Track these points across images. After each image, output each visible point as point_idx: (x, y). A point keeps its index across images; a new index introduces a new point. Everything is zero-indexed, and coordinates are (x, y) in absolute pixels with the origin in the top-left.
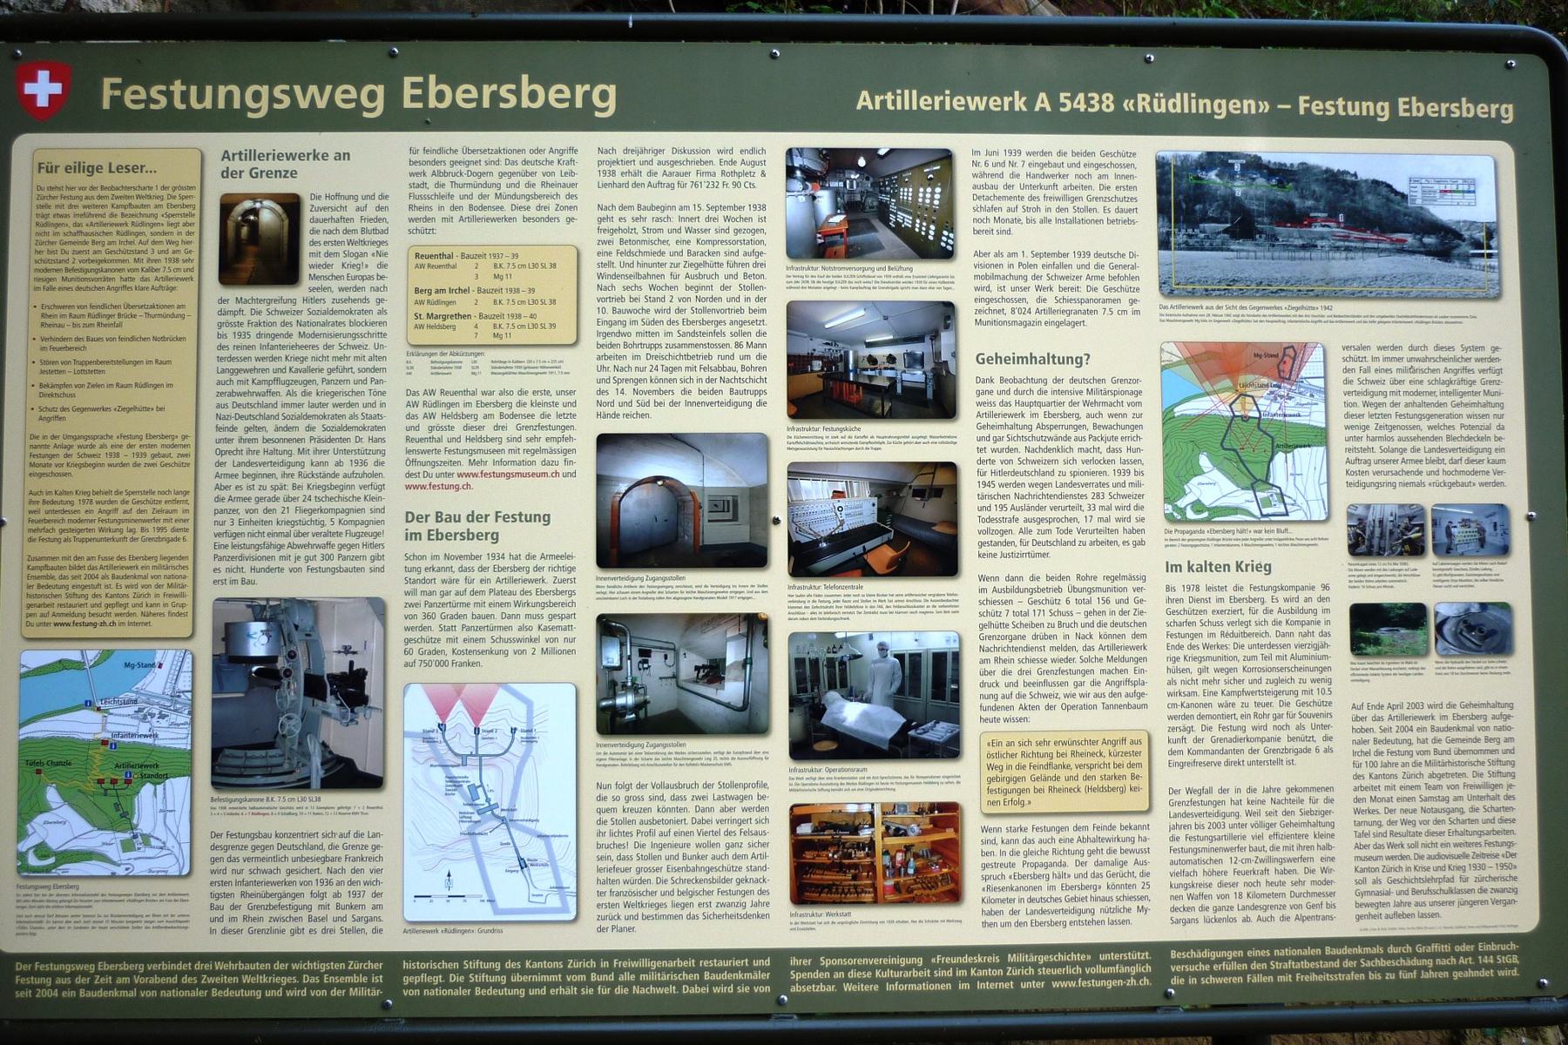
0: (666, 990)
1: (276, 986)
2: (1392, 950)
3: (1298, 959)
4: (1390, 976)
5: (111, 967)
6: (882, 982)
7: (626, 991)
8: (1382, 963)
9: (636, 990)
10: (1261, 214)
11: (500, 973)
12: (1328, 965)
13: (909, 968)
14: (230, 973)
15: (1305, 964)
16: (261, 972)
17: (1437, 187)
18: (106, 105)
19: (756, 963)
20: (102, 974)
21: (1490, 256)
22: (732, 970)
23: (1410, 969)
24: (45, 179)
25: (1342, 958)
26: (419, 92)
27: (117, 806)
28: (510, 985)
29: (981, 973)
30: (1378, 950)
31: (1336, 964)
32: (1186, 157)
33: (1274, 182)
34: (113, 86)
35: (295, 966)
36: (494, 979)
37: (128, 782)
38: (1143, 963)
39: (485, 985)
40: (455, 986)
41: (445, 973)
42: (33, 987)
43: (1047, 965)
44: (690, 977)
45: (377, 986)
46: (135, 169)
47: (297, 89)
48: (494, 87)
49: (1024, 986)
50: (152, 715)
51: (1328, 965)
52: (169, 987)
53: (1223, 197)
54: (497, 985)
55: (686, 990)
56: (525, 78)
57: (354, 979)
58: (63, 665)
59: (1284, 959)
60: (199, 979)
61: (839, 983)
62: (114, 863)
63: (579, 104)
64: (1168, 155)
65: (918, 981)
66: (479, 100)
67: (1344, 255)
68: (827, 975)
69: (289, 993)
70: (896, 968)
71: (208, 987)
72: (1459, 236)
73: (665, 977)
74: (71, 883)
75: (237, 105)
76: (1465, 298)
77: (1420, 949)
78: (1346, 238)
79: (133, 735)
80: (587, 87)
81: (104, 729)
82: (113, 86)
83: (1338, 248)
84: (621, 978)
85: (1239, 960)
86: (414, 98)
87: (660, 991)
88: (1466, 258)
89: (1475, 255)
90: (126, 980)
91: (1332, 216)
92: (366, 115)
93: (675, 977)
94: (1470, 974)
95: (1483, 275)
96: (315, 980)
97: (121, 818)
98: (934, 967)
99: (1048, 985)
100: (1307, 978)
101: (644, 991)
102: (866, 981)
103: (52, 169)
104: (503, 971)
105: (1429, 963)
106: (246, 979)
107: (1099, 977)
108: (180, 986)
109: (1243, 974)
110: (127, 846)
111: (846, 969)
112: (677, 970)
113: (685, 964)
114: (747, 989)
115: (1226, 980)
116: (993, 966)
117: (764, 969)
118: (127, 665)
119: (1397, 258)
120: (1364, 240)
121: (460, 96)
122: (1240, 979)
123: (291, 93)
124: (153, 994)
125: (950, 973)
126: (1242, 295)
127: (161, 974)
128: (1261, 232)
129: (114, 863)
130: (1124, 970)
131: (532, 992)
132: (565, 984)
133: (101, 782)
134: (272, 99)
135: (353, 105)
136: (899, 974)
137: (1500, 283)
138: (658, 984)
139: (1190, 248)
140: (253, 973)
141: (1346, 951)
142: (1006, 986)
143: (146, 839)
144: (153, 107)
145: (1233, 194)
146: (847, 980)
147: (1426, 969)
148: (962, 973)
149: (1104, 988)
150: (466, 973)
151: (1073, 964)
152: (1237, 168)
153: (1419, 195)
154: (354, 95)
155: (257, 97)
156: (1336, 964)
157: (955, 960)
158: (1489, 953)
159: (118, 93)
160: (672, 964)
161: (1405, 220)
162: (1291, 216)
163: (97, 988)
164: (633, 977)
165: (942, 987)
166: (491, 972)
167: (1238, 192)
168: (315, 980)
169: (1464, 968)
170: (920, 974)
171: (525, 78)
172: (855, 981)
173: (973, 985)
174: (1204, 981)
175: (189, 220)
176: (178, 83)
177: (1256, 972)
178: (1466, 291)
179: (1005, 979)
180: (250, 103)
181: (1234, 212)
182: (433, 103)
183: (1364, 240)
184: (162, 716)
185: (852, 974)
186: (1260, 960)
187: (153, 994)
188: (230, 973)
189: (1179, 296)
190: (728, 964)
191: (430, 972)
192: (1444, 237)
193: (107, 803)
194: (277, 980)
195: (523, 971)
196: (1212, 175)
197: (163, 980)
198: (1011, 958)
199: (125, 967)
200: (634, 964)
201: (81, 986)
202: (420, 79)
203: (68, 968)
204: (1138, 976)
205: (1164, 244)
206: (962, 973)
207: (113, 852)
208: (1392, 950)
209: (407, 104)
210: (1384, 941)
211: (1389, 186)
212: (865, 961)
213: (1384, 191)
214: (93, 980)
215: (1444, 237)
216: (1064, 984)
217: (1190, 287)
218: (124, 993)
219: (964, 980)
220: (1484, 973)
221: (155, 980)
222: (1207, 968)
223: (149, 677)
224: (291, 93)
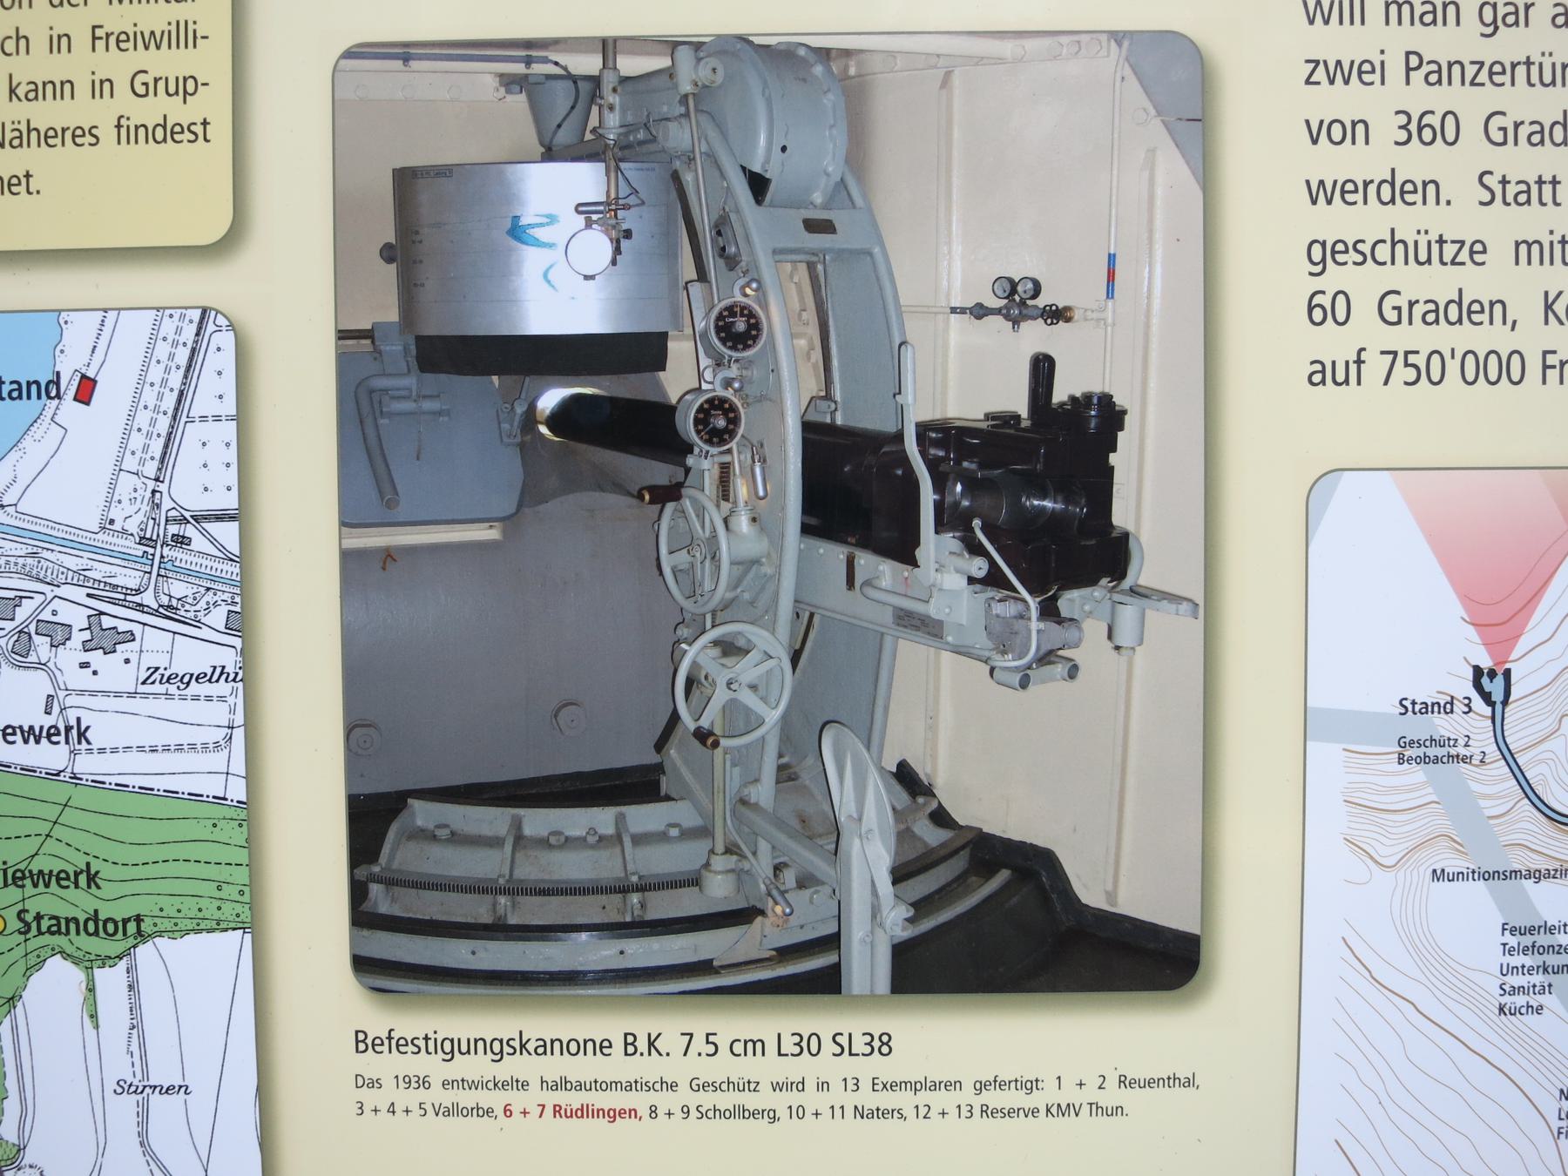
50: (58, 634)
184: (104, 640)
223: (36, 449)
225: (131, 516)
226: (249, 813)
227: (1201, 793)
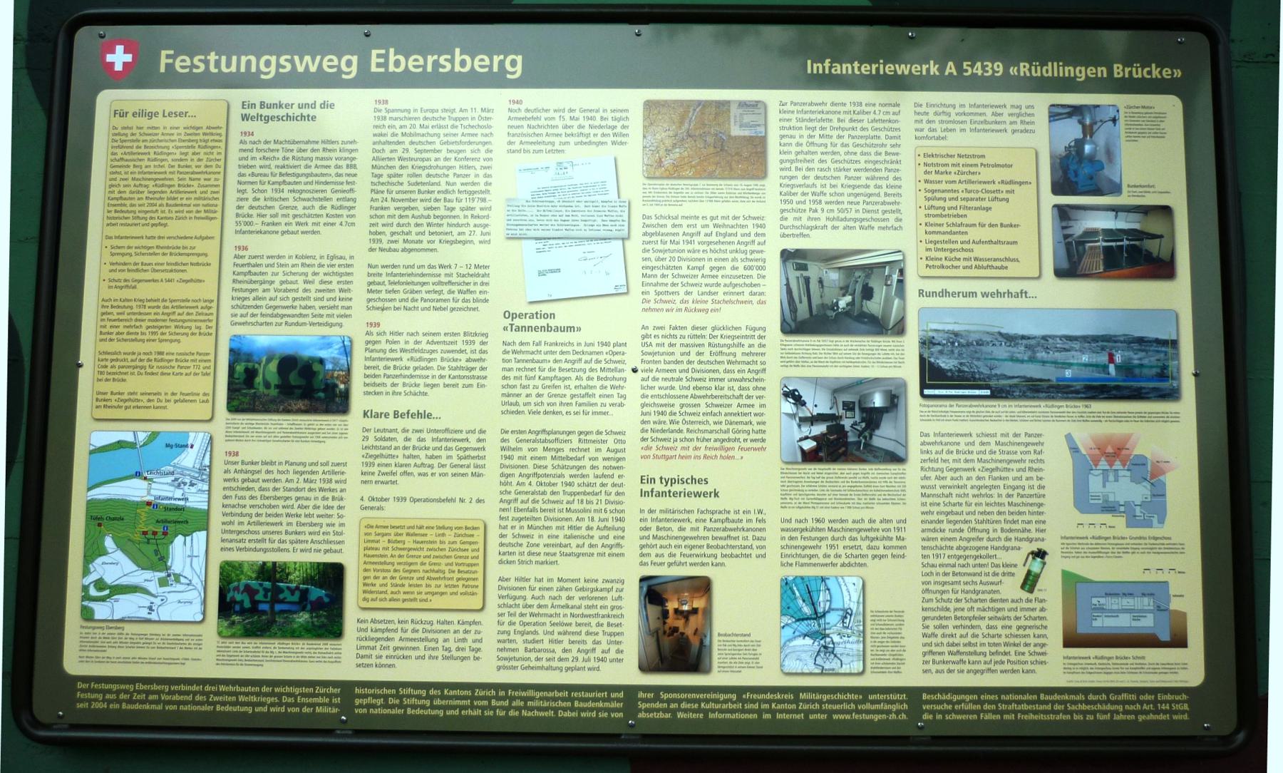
0: (546, 714)
2: (1091, 697)
5: (145, 687)
6: (706, 712)
7: (517, 713)
8: (1084, 707)
9: (524, 713)
11: (425, 698)
12: (1042, 707)
13: (726, 701)
15: (1025, 707)
16: (252, 694)
18: (162, 69)
19: (613, 695)
20: (139, 692)
22: (595, 700)
23: (1105, 712)
25: (1053, 702)
26: (382, 60)
27: (157, 552)
28: (433, 707)
29: (780, 707)
30: (1081, 697)
31: (1049, 707)
34: (168, 57)
35: (277, 690)
37: (165, 534)
38: (901, 702)
39: (414, 707)
40: (392, 707)
41: (386, 697)
42: (90, 701)
43: (830, 702)
44: (564, 704)
45: (336, 706)
48: (435, 57)
50: (185, 484)
51: (1042, 707)
54: (423, 707)
55: (561, 714)
57: (320, 700)
58: (120, 444)
61: (674, 712)
63: (495, 69)
68: (665, 705)
69: (272, 709)
70: (716, 701)
73: (546, 704)
79: (170, 499)
80: (502, 57)
81: (149, 494)
82: (168, 57)
84: (514, 704)
85: (974, 702)
86: (378, 65)
87: (542, 714)
90: (155, 697)
93: (553, 704)
94: (1151, 717)
96: (291, 700)
98: (744, 702)
99: (830, 717)
100: (1026, 717)
101: (530, 714)
102: (694, 711)
104: (428, 697)
105: (1120, 708)
107: (868, 712)
109: (977, 712)
110: (163, 583)
111: (679, 701)
113: (560, 694)
114: (606, 715)
115: (964, 717)
116: (789, 702)
117: (618, 700)
118: (167, 446)
121: (411, 63)
122: (975, 717)
124: (175, 707)
127: (181, 693)
131: (449, 713)
132: (473, 707)
133: (145, 533)
134: (279, 66)
136: (718, 706)
138: (540, 709)
140: (247, 694)
141: (1056, 697)
142: (798, 717)
143: (177, 577)
144: (195, 71)
146: (679, 710)
147: (1117, 712)
148: (766, 706)
149: (872, 721)
150: (401, 697)
151: (849, 702)
154: (336, 62)
155: (268, 64)
156: (1049, 707)
158: (1166, 702)
159: (170, 61)
160: (551, 694)
163: (134, 702)
164: (522, 704)
165: (750, 716)
166: (419, 697)
168: (291, 700)
172: (686, 711)
177: (988, 711)
179: (797, 711)
180: (344, 68)
182: (392, 68)
184: (192, 485)
185: (684, 705)
186: (990, 702)
187: (175, 707)
190: (592, 695)
191: (375, 696)
194: (263, 699)
195: (443, 697)
197: (181, 698)
198: (802, 696)
199: (155, 687)
200: (524, 694)
202: (383, 52)
203: (115, 687)
204: (898, 712)
206: (766, 706)
207: (153, 587)
208: (1091, 697)
209: (374, 69)
212: (694, 696)
216: (842, 717)
218: (153, 707)
219: (767, 711)
220: (1162, 717)
221: (176, 698)
222: (950, 707)
223: (183, 456)
225: (197, 466)
226: (208, 512)
227: (54, 363)
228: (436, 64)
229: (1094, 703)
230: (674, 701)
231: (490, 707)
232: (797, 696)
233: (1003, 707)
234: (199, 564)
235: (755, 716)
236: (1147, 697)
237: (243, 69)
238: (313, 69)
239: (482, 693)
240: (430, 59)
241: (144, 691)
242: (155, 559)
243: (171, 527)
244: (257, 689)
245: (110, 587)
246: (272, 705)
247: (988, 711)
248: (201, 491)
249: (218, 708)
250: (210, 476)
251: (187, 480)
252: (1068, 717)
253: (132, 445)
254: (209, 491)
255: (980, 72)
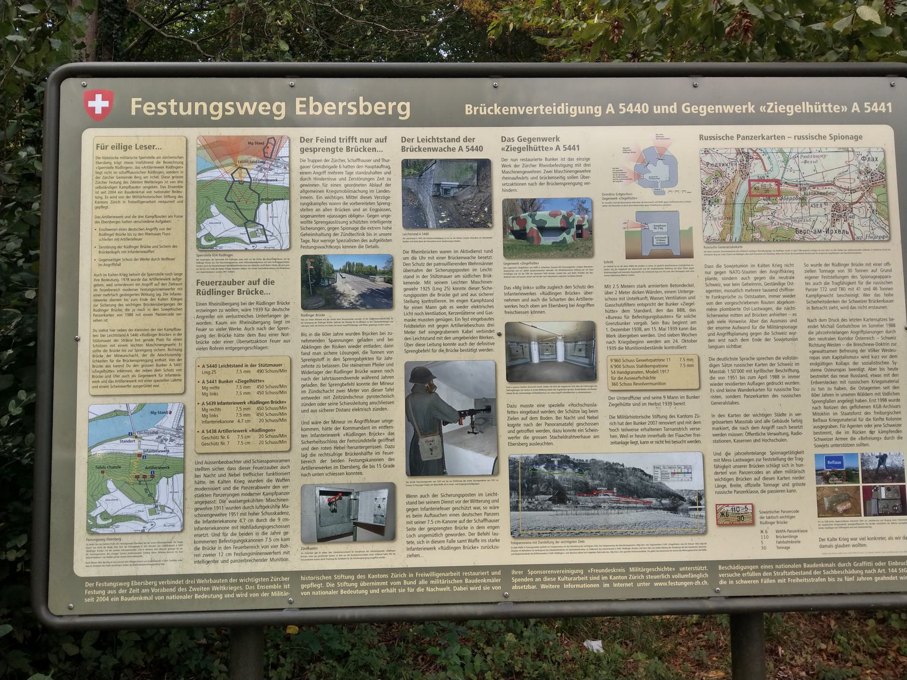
0: (444, 589)
1: (231, 592)
2: (840, 565)
3: (789, 570)
4: (840, 580)
5: (139, 584)
6: (561, 583)
7: (423, 590)
8: (835, 572)
9: (428, 589)
10: (569, 489)
11: (354, 582)
12: (805, 573)
13: (576, 575)
14: (205, 585)
15: (793, 573)
16: (222, 584)
17: (669, 471)
18: (133, 113)
19: (493, 573)
20: (134, 587)
21: (700, 509)
22: (480, 577)
23: (851, 575)
24: (100, 153)
25: (813, 569)
26: (304, 106)
27: (146, 490)
28: (360, 588)
29: (615, 578)
30: (832, 565)
31: (810, 573)
32: (527, 458)
33: (577, 470)
34: (137, 103)
35: (241, 580)
36: (351, 585)
37: (153, 477)
38: (703, 572)
39: (346, 588)
40: (329, 589)
41: (324, 582)
42: (95, 596)
43: (652, 573)
44: (457, 582)
45: (287, 590)
46: (149, 147)
47: (238, 104)
48: (345, 103)
49: (639, 585)
50: (166, 440)
51: (805, 573)
52: (172, 594)
53: (548, 480)
54: (353, 588)
55: (455, 589)
56: (361, 98)
57: (274, 587)
58: (116, 413)
59: (781, 570)
60: (188, 589)
61: (538, 584)
62: (144, 521)
63: (390, 112)
64: (517, 457)
65: (581, 582)
66: (337, 110)
67: (617, 511)
68: (532, 579)
69: (238, 595)
70: (569, 575)
71: (193, 593)
72: (682, 499)
73: (444, 582)
74: (117, 537)
75: (205, 113)
76: (686, 534)
77: (856, 565)
78: (617, 502)
79: (155, 451)
80: (395, 103)
81: (139, 448)
82: (137, 103)
83: (613, 508)
84: (420, 583)
85: (756, 571)
86: (301, 109)
87: (441, 589)
88: (686, 511)
89: (691, 509)
90: (147, 591)
91: (610, 489)
92: (275, 118)
93: (449, 582)
94: (884, 578)
95: (696, 521)
96: (252, 588)
97: (149, 497)
98: (589, 575)
99: (652, 585)
100: (794, 581)
101: (432, 590)
102: (553, 583)
103: (104, 148)
104: (356, 580)
105: (861, 572)
106: (215, 588)
107: (680, 580)
108: (177, 593)
109: (758, 578)
110: (152, 512)
111: (542, 576)
112: (450, 578)
113: (455, 574)
114: (488, 588)
115: (749, 582)
116: (622, 574)
117: (497, 577)
118: (152, 413)
119: (647, 512)
120: (628, 502)
121: (326, 108)
122: (757, 581)
123: (235, 107)
124: (162, 598)
125: (598, 578)
126: (559, 535)
127: (167, 586)
128: (569, 500)
129: (144, 521)
130: (693, 576)
131: (372, 592)
132: (389, 587)
133: (137, 477)
134: (224, 110)
135: (268, 113)
136: (571, 579)
137: (706, 525)
138: (440, 586)
139: (529, 509)
140: (218, 585)
141: (815, 565)
142: (629, 585)
143: (163, 508)
144: (159, 114)
145: (554, 480)
146: (543, 582)
147: (859, 575)
148: (605, 578)
149: (683, 586)
150: (335, 582)
151: (665, 573)
152: (556, 463)
153: (659, 476)
154: (269, 107)
155: (216, 108)
156: (810, 573)
157: (602, 571)
158: (894, 567)
159: (140, 106)
160: (447, 575)
161: (652, 491)
162: (587, 490)
163: (131, 595)
164: (426, 582)
165: (594, 586)
166: (349, 581)
167: (557, 477)
168: (252, 588)
169: (880, 575)
170: (582, 579)
171: (361, 98)
172: (547, 583)
173: (611, 585)
174: (737, 582)
175: (181, 180)
176: (173, 101)
177: (766, 577)
178: (687, 530)
179: (628, 581)
180: (212, 112)
181: (554, 488)
182: (312, 112)
183: (628, 502)
184: (172, 440)
185: (545, 579)
186: (768, 570)
187: (162, 598)
188: (205, 585)
189: (523, 538)
190: (478, 574)
191: (315, 582)
192: (674, 499)
193: (141, 489)
194: (231, 588)
195: (367, 580)
196: (542, 467)
197: (167, 590)
198: (632, 570)
199: (147, 583)
200: (427, 575)
201: (122, 594)
202: (305, 99)
203: (114, 585)
204: (701, 580)
205: (514, 508)
206: (605, 578)
207: (144, 516)
208: (840, 565)
209: (298, 112)
210: (836, 560)
211: (642, 471)
212: (552, 571)
213: (639, 474)
214: (128, 591)
215: (674, 499)
216: (661, 584)
217: (530, 532)
218: (146, 598)
219: (606, 582)
220: (892, 578)
221: (164, 590)
222: (739, 575)
223: (164, 419)
224: (235, 107)
225: (175, 427)
228: (345, 108)
229: (842, 569)
230: (538, 576)
231: (403, 586)
232: (627, 570)
233: (777, 574)
234: (179, 497)
235: (597, 585)
236: (881, 564)
237: (197, 113)
238: (251, 112)
239: (396, 576)
240: (341, 105)
241: (137, 587)
242: (146, 495)
243: (157, 472)
244: (226, 581)
245: (216, 239)
246: (238, 592)
247: (766, 577)
248: (179, 445)
249: (196, 596)
250: (184, 433)
251: (168, 437)
252: (824, 580)
253: (126, 413)
254: (184, 444)
255: (884, 110)
